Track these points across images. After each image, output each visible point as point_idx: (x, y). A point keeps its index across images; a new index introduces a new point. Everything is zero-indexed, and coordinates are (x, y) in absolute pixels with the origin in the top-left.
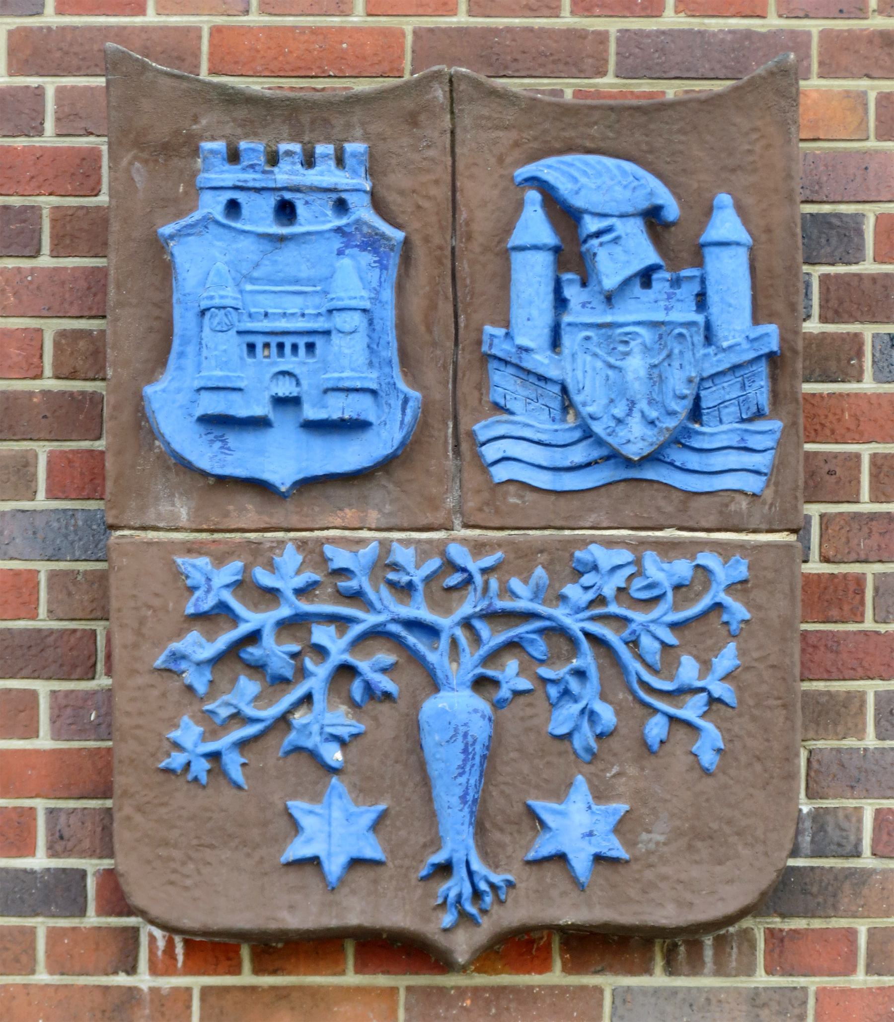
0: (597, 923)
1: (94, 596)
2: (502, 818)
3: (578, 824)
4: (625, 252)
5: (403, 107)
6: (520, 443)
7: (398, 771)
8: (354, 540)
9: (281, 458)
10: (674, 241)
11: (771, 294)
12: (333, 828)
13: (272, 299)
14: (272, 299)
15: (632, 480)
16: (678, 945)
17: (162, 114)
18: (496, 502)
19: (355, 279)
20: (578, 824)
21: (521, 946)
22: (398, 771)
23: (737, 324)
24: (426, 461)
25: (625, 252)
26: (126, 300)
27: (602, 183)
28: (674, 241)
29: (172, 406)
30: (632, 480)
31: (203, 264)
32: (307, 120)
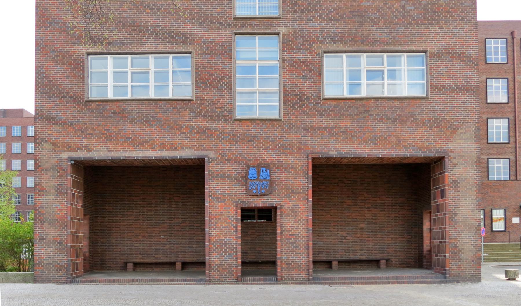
0: (410, 161)
1: (246, 183)
2: (260, 191)
3: (263, 191)
4: (265, 171)
5: (256, 166)
6: (261, 178)
7: (257, 189)
8: (255, 181)
9: (253, 179)
10: (266, 171)
11: (270, 173)
12: (255, 191)
13: (252, 173)
14: (252, 173)
15: (265, 179)
16: (266, 195)
17: (248, 167)
18: (260, 180)
19: (255, 172)
20: (263, 191)
21: (261, 195)
22: (257, 189)
23: (268, 174)
24: (258, 179)
25: (265, 171)
26: (247, 173)
27: (264, 169)
28: (266, 171)
29: (249, 177)
30: (265, 179)
31: (250, 172)
32: (253, 167)
